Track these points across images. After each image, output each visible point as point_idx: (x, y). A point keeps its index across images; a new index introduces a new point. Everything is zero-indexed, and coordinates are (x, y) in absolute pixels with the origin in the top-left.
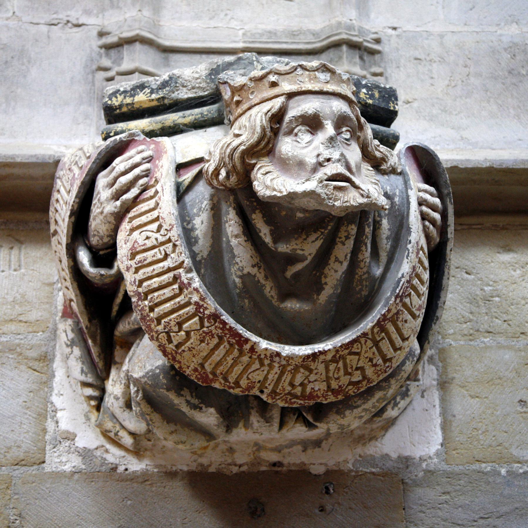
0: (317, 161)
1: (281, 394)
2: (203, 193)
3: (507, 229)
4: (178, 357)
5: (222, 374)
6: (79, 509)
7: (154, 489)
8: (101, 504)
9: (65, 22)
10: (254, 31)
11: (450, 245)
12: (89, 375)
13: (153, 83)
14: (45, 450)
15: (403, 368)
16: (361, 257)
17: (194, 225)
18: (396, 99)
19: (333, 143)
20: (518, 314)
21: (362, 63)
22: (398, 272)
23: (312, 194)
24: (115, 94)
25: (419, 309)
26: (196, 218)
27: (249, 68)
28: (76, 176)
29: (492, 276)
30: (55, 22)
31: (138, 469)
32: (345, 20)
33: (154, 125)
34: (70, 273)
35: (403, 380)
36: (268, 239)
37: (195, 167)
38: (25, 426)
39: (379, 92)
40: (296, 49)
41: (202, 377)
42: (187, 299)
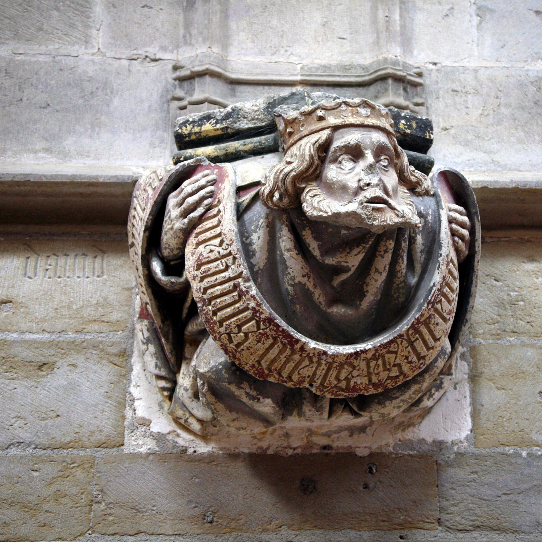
0: (359, 185)
1: (328, 387)
2: (259, 212)
3: (531, 241)
4: (238, 355)
5: (276, 370)
6: (153, 485)
7: (219, 468)
8: (173, 482)
9: (144, 57)
10: (311, 66)
11: (478, 257)
12: (162, 369)
13: (218, 114)
14: (124, 434)
15: (436, 365)
16: (398, 268)
17: (252, 240)
18: (432, 129)
19: (372, 169)
20: (539, 316)
21: (405, 95)
22: (430, 281)
23: (353, 214)
24: (185, 123)
25: (449, 314)
26: (254, 234)
27: (301, 102)
28: (150, 196)
29: (517, 283)
30: (135, 57)
31: (205, 451)
32: (391, 56)
33: (219, 151)
34: (145, 280)
35: (436, 375)
36: (316, 253)
37: (253, 189)
38: (106, 414)
39: (417, 123)
40: (347, 82)
41: (259, 373)
42: (245, 305)
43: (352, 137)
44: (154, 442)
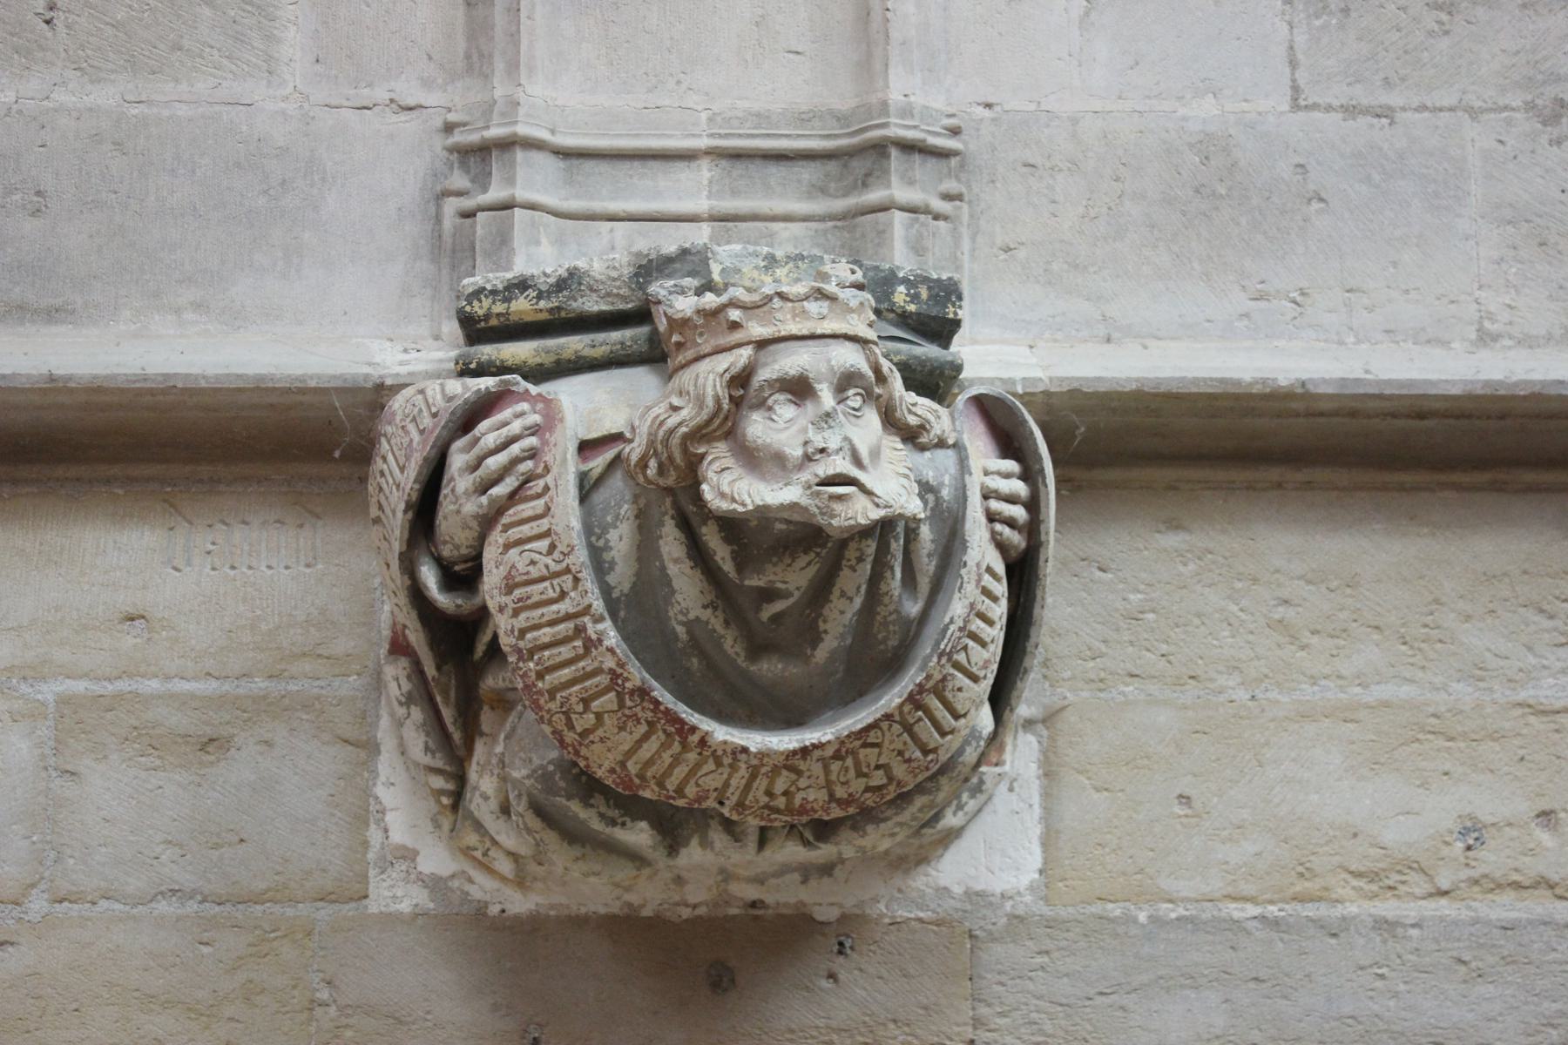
3: (1175, 488)
4: (583, 751)
16: (883, 588)
17: (607, 541)
18: (960, 298)
23: (794, 506)
36: (728, 567)
39: (929, 288)
41: (623, 782)
42: (596, 664)
43: (792, 361)
44: (426, 892)
